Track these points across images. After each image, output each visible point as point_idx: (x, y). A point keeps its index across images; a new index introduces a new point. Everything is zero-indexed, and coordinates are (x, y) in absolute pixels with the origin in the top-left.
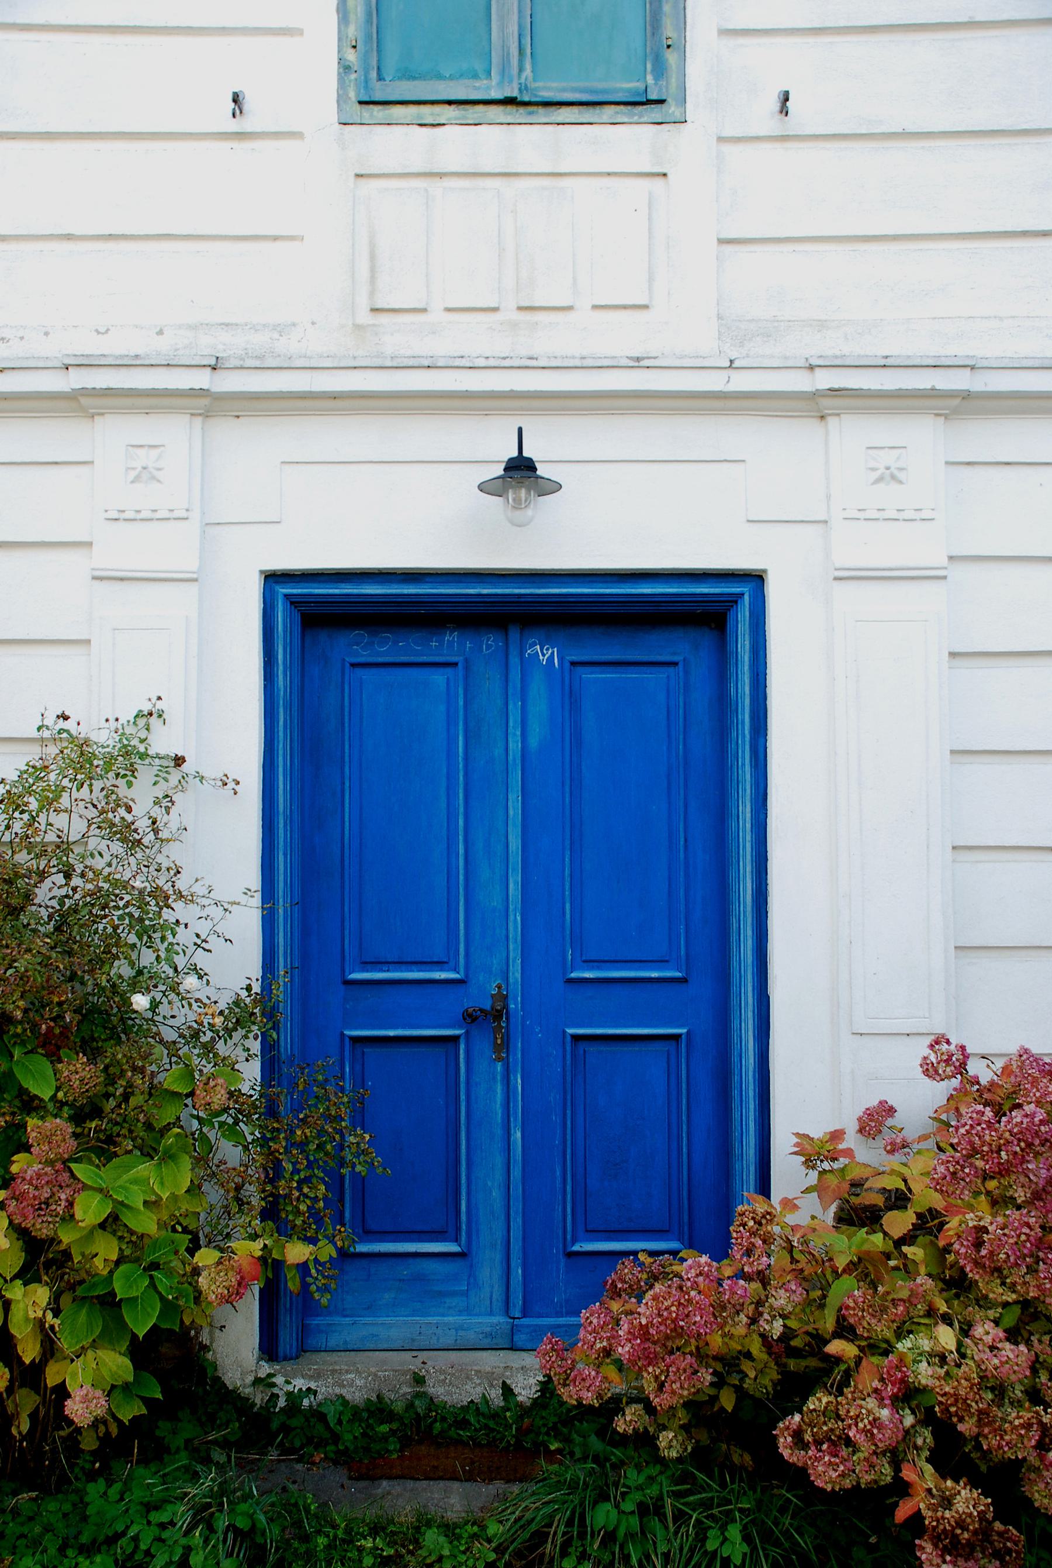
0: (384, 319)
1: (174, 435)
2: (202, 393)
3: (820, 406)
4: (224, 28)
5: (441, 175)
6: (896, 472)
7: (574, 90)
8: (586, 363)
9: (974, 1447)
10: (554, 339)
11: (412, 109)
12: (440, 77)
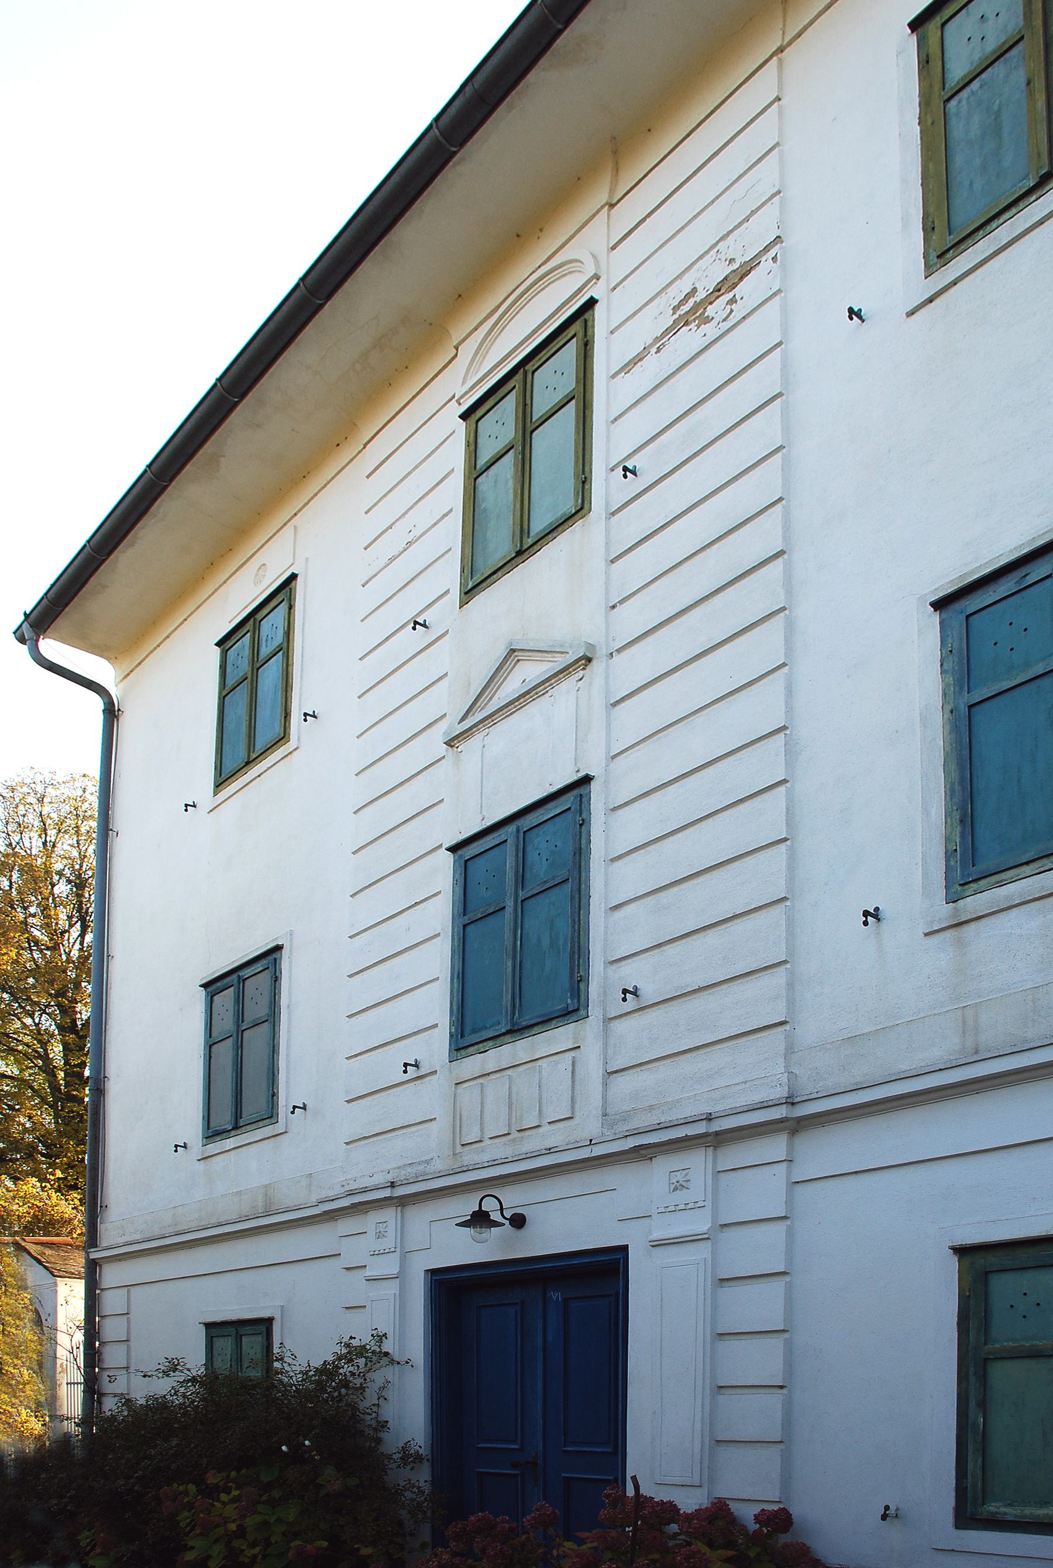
0: (467, 1148)
1: (389, 1216)
2: (705, 1135)
3: (643, 1154)
4: (931, 301)
5: (488, 1074)
6: (684, 1184)
7: (537, 1017)
8: (529, 1155)
9: (63, 997)
10: (533, 1143)
11: (476, 1047)
12: (486, 1028)
